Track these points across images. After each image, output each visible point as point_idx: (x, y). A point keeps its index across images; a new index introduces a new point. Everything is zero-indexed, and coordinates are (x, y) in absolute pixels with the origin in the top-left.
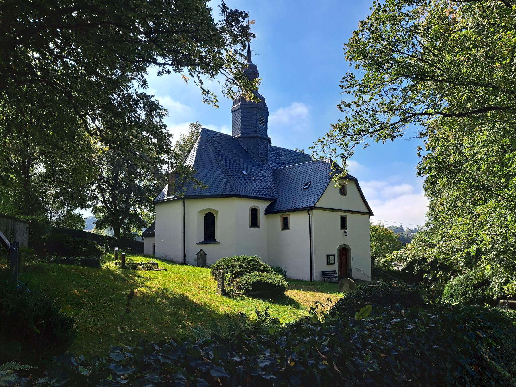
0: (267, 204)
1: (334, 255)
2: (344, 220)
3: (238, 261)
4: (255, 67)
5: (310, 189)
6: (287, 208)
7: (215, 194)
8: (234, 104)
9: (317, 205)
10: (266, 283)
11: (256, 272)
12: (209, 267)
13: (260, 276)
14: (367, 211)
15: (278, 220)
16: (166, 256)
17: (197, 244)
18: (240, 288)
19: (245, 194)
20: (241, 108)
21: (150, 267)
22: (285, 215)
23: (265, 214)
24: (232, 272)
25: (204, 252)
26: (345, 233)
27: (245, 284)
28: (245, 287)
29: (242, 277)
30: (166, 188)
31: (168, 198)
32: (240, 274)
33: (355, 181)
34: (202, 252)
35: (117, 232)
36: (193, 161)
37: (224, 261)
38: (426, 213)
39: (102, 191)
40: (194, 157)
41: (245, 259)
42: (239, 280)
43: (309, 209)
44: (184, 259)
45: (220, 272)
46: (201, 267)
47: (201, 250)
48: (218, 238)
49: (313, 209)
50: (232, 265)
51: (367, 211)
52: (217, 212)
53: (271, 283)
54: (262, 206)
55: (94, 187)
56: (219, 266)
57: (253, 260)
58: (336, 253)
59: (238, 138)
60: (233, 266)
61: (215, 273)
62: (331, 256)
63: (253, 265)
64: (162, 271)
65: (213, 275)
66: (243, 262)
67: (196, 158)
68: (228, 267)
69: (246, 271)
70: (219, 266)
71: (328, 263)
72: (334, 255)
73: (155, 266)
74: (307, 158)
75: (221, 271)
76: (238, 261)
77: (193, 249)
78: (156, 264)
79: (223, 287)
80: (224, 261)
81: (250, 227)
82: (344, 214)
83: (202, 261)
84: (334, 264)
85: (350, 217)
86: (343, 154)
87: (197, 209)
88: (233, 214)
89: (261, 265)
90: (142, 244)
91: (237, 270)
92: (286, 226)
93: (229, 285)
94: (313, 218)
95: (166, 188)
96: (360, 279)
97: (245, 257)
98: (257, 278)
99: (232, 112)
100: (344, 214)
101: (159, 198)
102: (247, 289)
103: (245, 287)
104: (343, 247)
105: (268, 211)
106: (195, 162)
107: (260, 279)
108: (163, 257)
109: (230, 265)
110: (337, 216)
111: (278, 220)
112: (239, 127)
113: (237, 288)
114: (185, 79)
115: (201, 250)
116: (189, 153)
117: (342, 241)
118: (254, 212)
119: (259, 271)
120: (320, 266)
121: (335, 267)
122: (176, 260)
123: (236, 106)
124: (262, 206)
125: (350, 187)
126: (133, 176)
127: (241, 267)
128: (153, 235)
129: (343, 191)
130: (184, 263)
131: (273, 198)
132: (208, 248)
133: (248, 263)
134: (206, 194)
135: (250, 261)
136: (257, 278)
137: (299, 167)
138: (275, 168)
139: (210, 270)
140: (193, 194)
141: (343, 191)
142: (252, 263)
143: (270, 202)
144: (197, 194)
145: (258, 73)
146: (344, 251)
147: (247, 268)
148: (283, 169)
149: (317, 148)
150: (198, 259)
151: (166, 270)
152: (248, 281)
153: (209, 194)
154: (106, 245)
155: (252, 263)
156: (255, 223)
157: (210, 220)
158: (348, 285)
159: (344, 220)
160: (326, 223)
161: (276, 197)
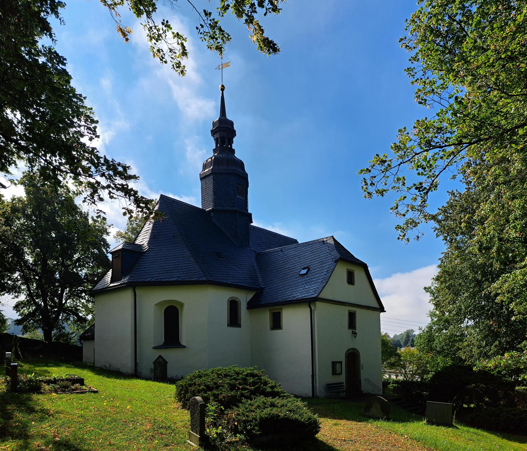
0: (250, 296)
1: (341, 362)
2: (352, 316)
3: (226, 376)
4: (231, 123)
5: (309, 275)
6: (280, 300)
7: (180, 279)
8: (204, 168)
9: (322, 296)
10: (287, 421)
11: (262, 399)
12: (172, 381)
13: (273, 405)
14: (377, 305)
15: (265, 317)
16: (110, 365)
17: (154, 348)
18: (235, 431)
19: (221, 281)
20: (213, 173)
21: (68, 386)
22: (276, 309)
23: (248, 308)
24: (216, 396)
25: (164, 360)
26: (355, 334)
27: (245, 422)
28: (245, 428)
29: (238, 407)
30: (110, 273)
31: (112, 285)
32: (230, 403)
33: (364, 267)
34: (161, 360)
35: (47, 334)
36: (148, 236)
37: (200, 377)
38: (428, 312)
39: (27, 281)
40: (150, 231)
41: (238, 374)
42: (232, 414)
43: (310, 302)
44: (136, 370)
45: (197, 402)
46: (160, 382)
47: (160, 356)
48: (184, 340)
49: (317, 300)
50: (215, 383)
51: (377, 305)
52: (182, 305)
53: (296, 420)
54: (244, 298)
55: (16, 275)
56: (190, 385)
57: (253, 375)
58: (343, 359)
59: (210, 211)
60: (217, 386)
61: (184, 397)
62: (338, 364)
63: (254, 384)
64: (87, 394)
65: (180, 400)
66: (234, 379)
67: (152, 233)
68: (209, 388)
69: (242, 395)
70: (190, 385)
71: (334, 373)
72: (341, 362)
73: (77, 385)
74: (295, 241)
75: (198, 398)
76: (226, 376)
77: (149, 356)
78: (81, 381)
79: (202, 431)
80: (200, 377)
81: (228, 325)
82: (353, 309)
83: (160, 373)
84: (341, 373)
85: (360, 314)
86: (421, 184)
87: (153, 300)
88: (203, 307)
89: (266, 383)
90: (80, 350)
91: (225, 393)
92: (276, 324)
93: (215, 425)
94: (316, 313)
95: (110, 273)
96: (370, 392)
97: (237, 369)
98: (268, 410)
99: (201, 179)
100: (353, 309)
101: (99, 286)
102: (249, 432)
103: (245, 428)
104: (351, 351)
105: (252, 305)
106: (150, 239)
107: (275, 411)
108: (105, 366)
109: (211, 384)
110: (345, 311)
111: (266, 317)
112: (211, 198)
113: (231, 430)
114: (124, 35)
115: (160, 356)
116: (143, 227)
117: (348, 343)
118: (233, 305)
119: (267, 395)
120: (325, 377)
121: (342, 378)
122: (124, 370)
123: (206, 171)
124: (244, 298)
125: (359, 274)
126: (69, 263)
127: (232, 387)
128: (92, 338)
129: (351, 280)
130: (136, 375)
131: (258, 287)
132: (170, 355)
133: (245, 380)
134: (166, 280)
135: (247, 375)
136: (268, 410)
137: (289, 250)
138: (258, 252)
139: (172, 389)
140: (147, 280)
141: (351, 280)
142: (251, 380)
143: (254, 293)
144: (153, 280)
145: (234, 132)
146: (353, 356)
147: (244, 389)
148: (269, 252)
149: (374, 172)
150: (155, 368)
151: (97, 392)
152: (252, 415)
153: (170, 280)
154: (16, 349)
155: (251, 380)
156: (234, 320)
157: (172, 315)
158: (379, 406)
159: (352, 316)
160: (335, 318)
161: (262, 286)
